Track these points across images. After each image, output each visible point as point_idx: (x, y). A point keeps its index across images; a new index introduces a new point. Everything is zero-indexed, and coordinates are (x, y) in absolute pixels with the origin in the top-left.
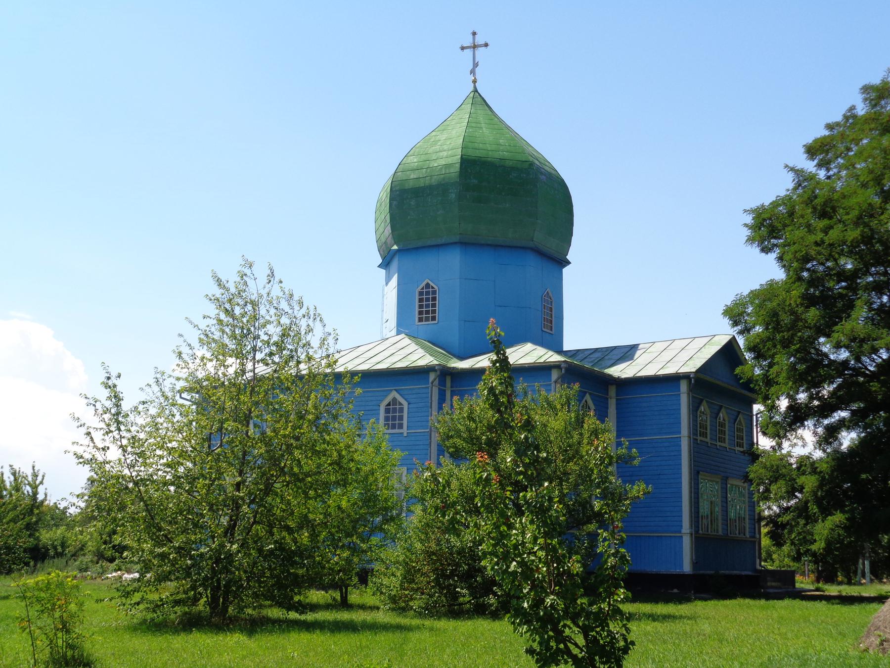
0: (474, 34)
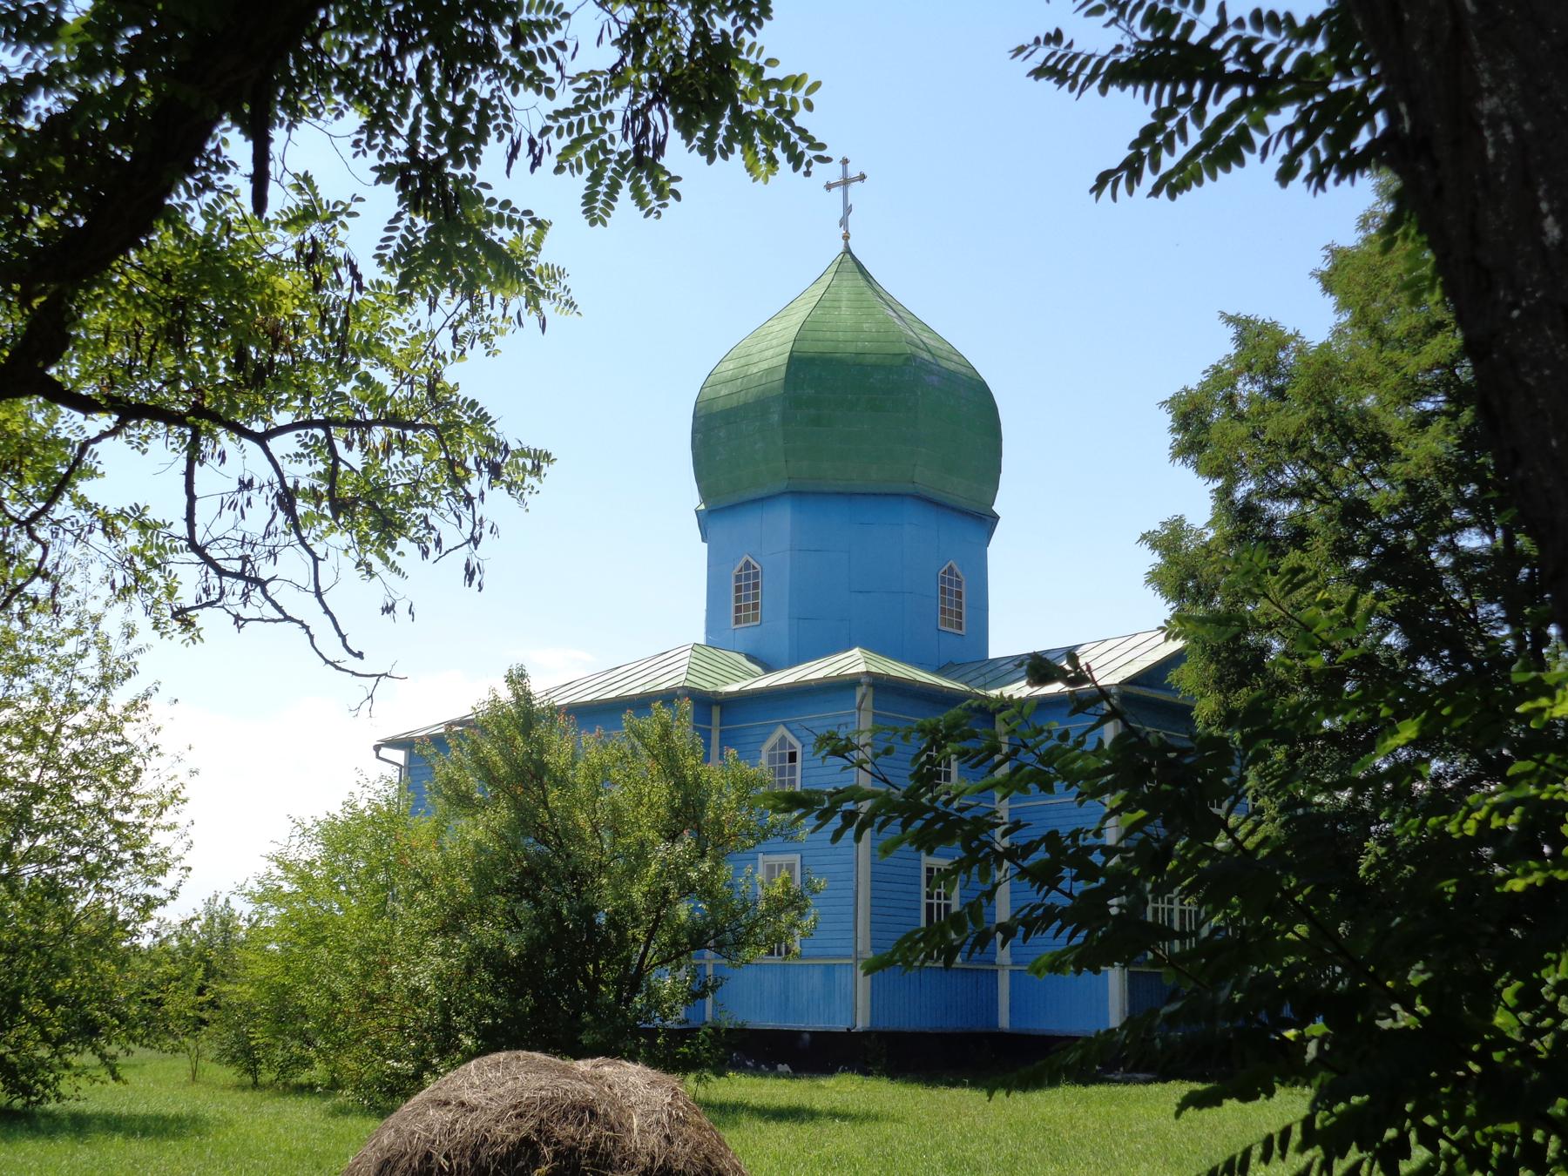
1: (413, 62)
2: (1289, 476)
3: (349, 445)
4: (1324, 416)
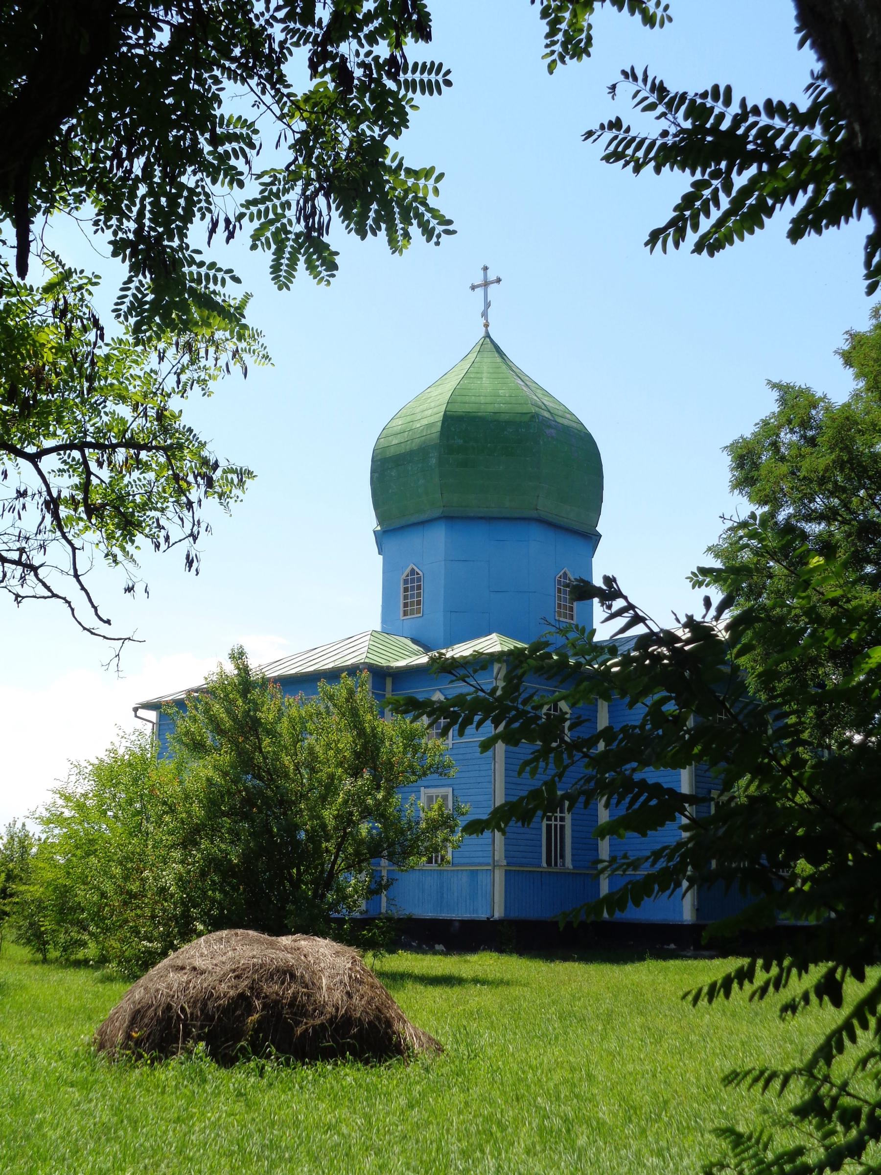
0: (486, 269)
1: (139, 164)
2: (819, 503)
3: (100, 464)
4: (845, 458)
